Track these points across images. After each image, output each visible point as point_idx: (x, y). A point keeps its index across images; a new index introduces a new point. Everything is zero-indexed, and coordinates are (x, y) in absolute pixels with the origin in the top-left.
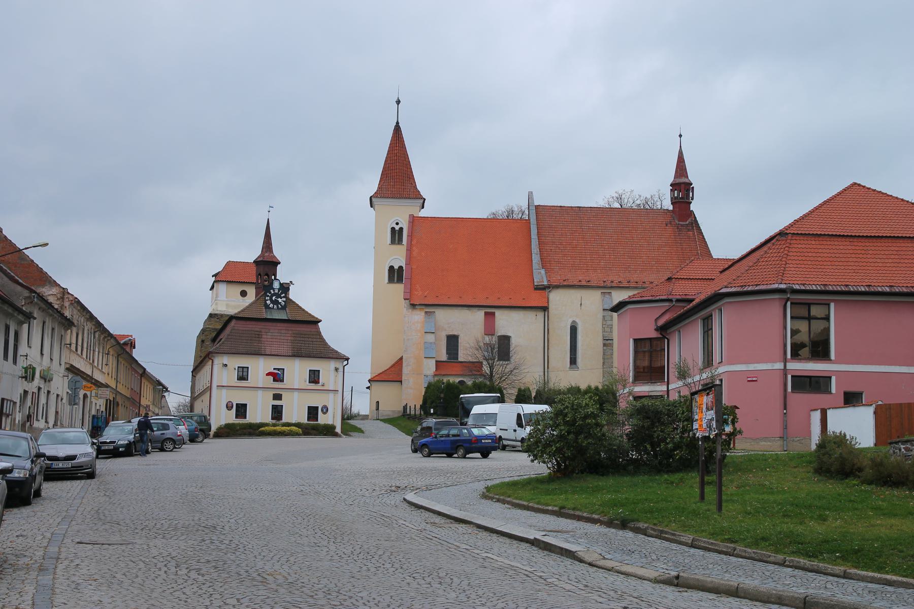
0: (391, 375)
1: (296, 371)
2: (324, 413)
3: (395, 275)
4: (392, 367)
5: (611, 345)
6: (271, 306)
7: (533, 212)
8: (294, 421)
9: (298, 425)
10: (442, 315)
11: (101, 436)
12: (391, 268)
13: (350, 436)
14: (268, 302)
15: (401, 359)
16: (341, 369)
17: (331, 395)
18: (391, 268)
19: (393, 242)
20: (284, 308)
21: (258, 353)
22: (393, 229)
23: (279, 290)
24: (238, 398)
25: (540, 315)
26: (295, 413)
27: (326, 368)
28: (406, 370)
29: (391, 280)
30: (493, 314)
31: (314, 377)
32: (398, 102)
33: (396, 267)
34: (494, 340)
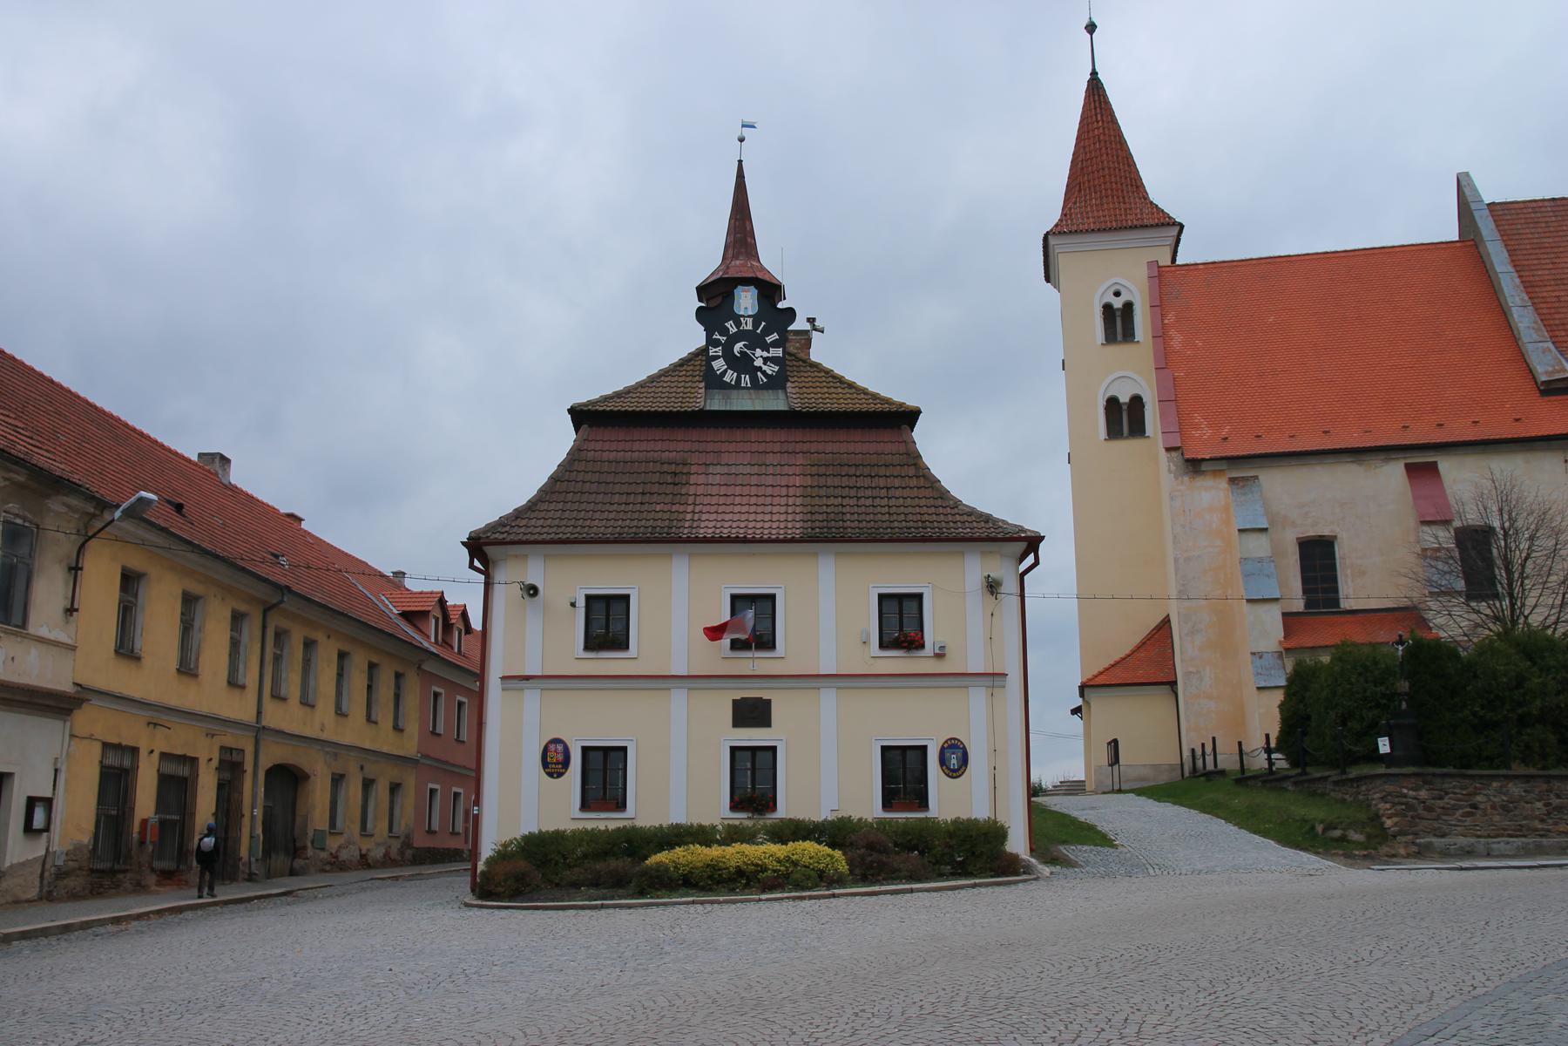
0: (1146, 667)
1: (829, 606)
2: (954, 773)
3: (1124, 418)
4: (1138, 648)
6: (730, 377)
7: (1487, 227)
8: (822, 812)
9: (836, 833)
10: (1278, 484)
12: (1112, 404)
13: (1067, 863)
14: (719, 365)
15: (1166, 621)
16: (1010, 585)
17: (977, 697)
18: (1112, 404)
19: (1110, 338)
20: (776, 383)
21: (666, 537)
22: (1107, 308)
23: (757, 319)
24: (588, 722)
26: (830, 776)
27: (948, 587)
28: (1186, 651)
29: (1114, 432)
30: (1432, 469)
31: (901, 622)
33: (1124, 399)
34: (1445, 537)
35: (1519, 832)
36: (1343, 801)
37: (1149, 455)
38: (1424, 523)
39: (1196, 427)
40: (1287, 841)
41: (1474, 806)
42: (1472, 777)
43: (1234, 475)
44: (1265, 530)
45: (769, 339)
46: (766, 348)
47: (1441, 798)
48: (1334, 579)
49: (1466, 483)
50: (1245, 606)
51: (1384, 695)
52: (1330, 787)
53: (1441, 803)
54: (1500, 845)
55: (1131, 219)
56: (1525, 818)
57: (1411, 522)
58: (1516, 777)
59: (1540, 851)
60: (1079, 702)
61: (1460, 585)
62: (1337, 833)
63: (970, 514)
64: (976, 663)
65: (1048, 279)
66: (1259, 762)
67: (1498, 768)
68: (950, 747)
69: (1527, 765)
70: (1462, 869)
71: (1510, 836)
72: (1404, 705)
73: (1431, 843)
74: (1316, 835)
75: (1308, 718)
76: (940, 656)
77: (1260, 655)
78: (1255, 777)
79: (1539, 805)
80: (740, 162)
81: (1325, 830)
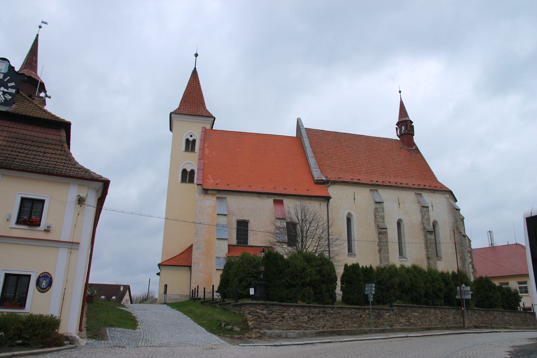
0: (181, 261)
2: (43, 290)
3: (187, 176)
5: (386, 233)
10: (233, 201)
11: (516, 290)
12: (184, 171)
15: (192, 246)
17: (63, 253)
18: (184, 171)
19: (187, 149)
22: (187, 140)
25: (324, 205)
27: (60, 203)
28: (196, 254)
29: (184, 180)
30: (281, 202)
31: (30, 212)
32: (196, 55)
33: (189, 170)
35: (298, 328)
36: (235, 313)
37: (192, 189)
38: (277, 218)
39: (209, 179)
40: (210, 330)
41: (283, 317)
42: (284, 306)
43: (219, 196)
44: (226, 215)
45: (10, 85)
46: (7, 88)
47: (271, 314)
48: (247, 235)
49: (291, 206)
50: (217, 241)
51: (256, 273)
52: (231, 307)
53: (271, 316)
54: (291, 333)
55: (199, 113)
56: (301, 322)
57: (273, 218)
58: (299, 306)
59: (305, 336)
60: (159, 271)
61: (286, 238)
62: (229, 327)
63: (79, 169)
64: (65, 237)
65: (171, 130)
66: (208, 296)
67: (293, 302)
68: (44, 276)
69: (303, 302)
70: (276, 346)
71: (295, 329)
72: (262, 276)
73: (265, 332)
74: (221, 327)
75: (229, 280)
76: (47, 231)
77: (219, 258)
78: (207, 301)
79: (306, 317)
80: (38, 35)
81: (225, 325)
